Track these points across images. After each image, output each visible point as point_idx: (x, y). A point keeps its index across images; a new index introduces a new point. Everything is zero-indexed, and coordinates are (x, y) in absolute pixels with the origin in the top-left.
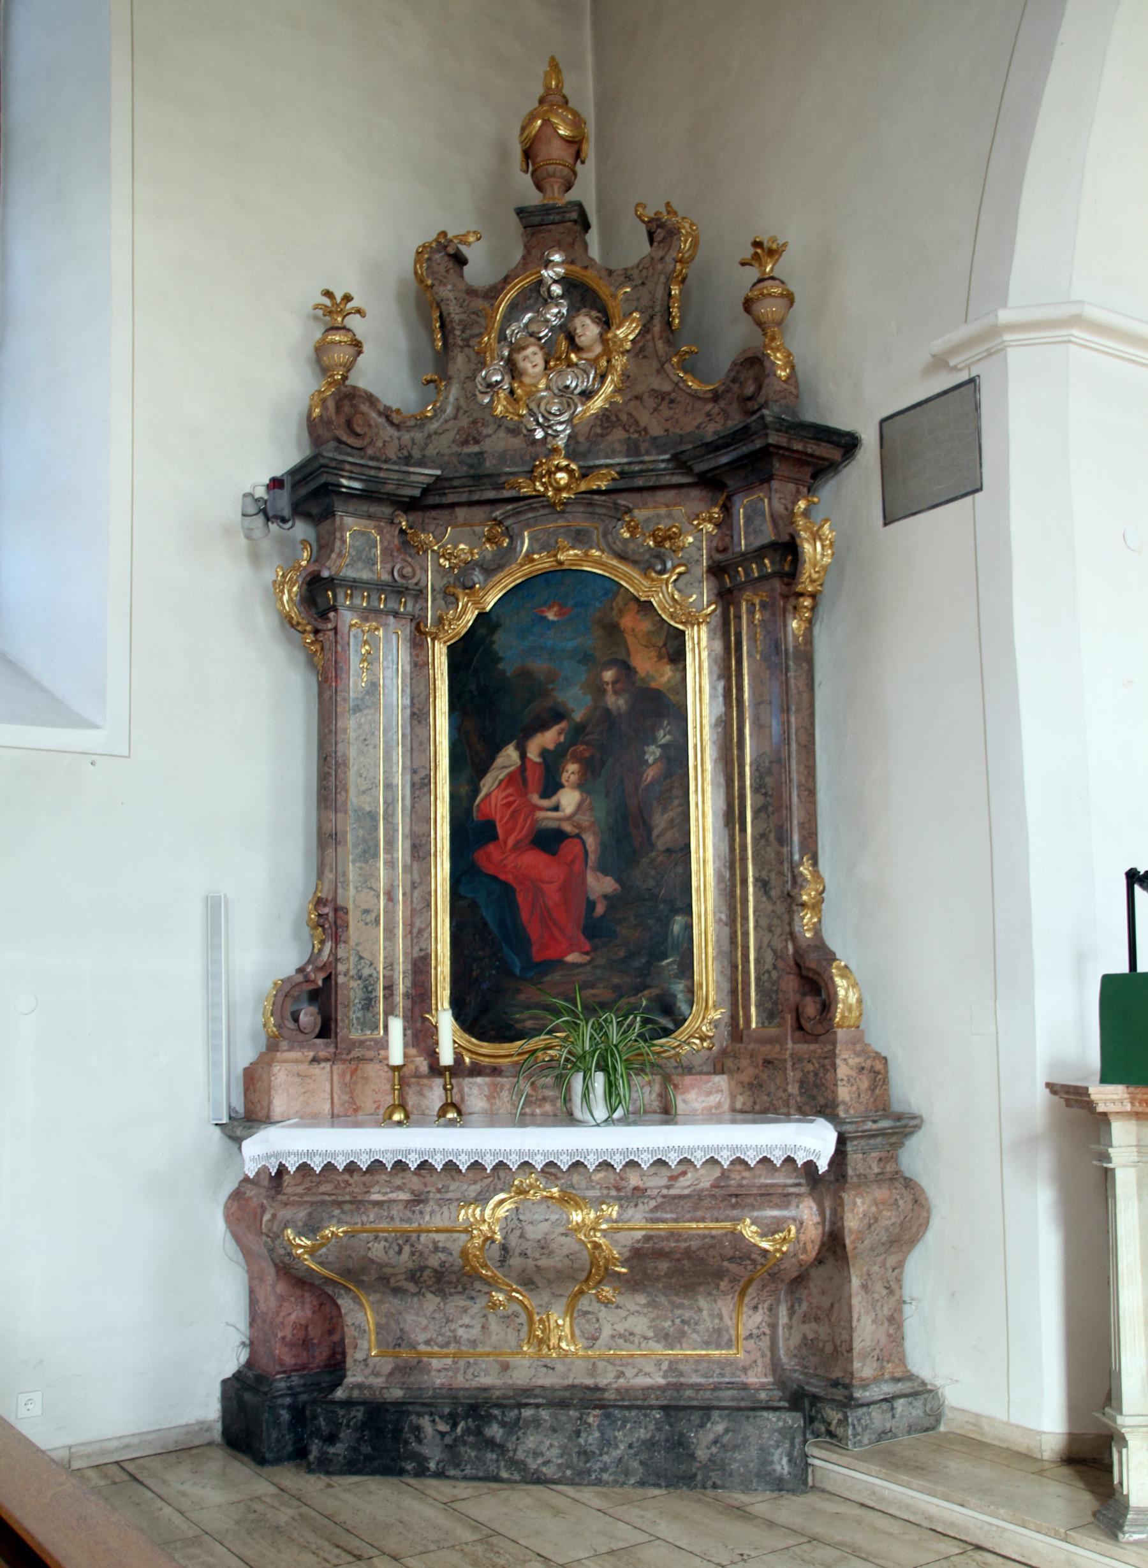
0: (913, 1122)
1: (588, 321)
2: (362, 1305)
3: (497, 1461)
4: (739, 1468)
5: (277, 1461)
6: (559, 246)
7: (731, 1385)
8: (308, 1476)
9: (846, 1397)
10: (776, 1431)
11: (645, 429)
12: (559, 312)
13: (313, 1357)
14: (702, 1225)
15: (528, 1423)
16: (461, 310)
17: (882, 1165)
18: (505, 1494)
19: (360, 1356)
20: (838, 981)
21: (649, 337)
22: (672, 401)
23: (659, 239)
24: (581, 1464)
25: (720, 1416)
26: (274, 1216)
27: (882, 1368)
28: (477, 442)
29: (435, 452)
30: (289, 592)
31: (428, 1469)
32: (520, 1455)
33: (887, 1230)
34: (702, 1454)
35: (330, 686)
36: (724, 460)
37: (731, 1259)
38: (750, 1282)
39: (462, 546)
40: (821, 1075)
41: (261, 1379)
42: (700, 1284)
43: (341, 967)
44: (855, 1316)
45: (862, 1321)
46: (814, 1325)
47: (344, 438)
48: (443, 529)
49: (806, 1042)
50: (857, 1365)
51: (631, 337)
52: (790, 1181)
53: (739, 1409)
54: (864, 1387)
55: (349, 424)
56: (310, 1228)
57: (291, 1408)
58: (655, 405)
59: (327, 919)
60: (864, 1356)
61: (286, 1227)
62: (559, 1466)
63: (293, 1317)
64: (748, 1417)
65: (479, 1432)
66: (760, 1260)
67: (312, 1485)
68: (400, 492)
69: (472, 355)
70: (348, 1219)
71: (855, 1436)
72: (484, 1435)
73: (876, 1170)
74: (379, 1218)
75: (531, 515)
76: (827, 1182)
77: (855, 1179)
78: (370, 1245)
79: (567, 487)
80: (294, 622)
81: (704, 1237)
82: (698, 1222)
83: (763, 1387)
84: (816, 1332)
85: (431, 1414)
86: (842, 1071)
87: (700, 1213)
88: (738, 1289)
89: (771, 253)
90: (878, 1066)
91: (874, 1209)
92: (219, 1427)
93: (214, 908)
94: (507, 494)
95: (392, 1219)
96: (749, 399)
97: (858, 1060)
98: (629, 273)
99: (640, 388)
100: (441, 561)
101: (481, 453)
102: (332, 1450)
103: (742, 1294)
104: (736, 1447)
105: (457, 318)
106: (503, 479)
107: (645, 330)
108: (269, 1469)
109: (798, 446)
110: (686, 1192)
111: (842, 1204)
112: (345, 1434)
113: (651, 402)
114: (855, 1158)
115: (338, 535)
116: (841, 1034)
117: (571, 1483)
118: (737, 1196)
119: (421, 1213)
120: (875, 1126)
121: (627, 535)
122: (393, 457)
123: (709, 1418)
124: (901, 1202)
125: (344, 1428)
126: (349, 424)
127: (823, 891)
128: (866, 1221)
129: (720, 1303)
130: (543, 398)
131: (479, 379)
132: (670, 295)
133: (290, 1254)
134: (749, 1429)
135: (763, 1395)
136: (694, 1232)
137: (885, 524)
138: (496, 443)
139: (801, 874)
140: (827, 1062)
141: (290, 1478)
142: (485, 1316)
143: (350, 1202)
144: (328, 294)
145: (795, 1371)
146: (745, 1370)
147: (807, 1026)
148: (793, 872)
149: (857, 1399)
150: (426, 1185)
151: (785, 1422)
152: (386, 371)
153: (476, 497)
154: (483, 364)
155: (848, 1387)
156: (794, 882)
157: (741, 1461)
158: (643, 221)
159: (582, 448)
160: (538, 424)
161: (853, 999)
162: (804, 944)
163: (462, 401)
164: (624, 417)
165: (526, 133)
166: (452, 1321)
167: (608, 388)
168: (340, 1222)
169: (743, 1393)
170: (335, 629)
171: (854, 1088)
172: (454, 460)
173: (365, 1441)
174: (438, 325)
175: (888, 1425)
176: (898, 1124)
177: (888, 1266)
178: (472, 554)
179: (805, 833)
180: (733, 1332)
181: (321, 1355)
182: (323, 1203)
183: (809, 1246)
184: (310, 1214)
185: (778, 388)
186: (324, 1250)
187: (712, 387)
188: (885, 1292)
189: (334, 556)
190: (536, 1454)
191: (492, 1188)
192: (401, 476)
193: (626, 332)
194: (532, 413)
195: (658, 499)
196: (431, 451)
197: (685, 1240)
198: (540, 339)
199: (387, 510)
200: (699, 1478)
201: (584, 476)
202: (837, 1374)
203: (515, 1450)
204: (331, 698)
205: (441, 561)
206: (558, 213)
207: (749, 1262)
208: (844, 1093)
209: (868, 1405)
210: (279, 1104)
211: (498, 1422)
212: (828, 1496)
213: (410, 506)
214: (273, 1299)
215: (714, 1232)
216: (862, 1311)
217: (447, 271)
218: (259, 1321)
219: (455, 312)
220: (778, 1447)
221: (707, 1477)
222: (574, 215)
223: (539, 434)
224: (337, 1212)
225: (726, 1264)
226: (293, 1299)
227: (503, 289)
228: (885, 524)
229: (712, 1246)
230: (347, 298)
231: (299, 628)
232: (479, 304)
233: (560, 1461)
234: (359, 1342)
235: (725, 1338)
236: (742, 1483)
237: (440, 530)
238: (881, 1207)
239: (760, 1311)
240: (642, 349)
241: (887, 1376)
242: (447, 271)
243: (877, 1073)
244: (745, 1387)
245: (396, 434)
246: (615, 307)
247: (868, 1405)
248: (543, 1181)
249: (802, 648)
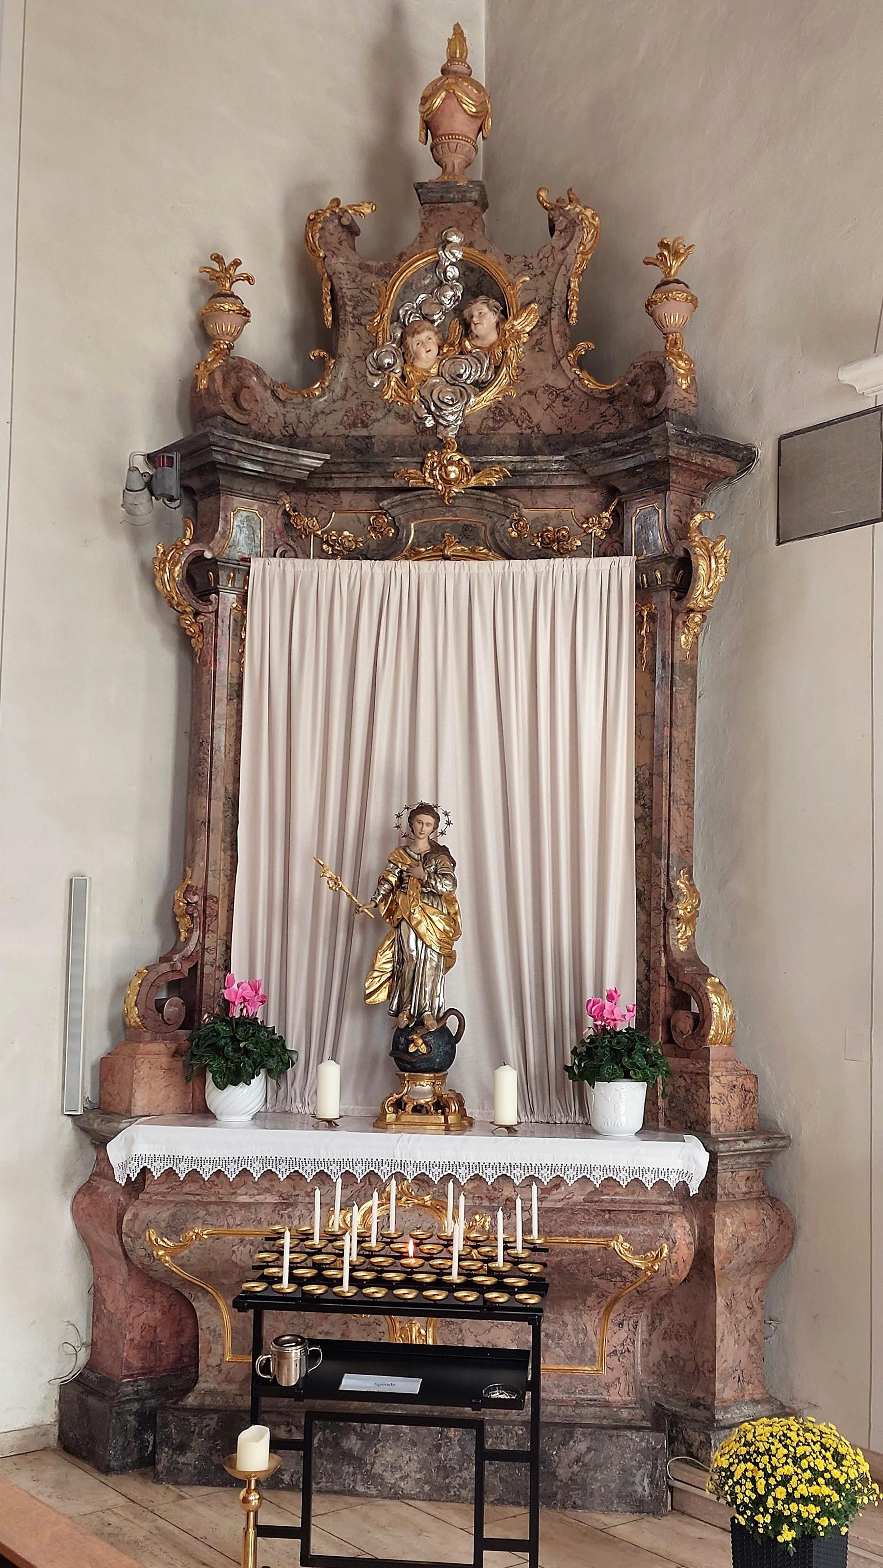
0: (782, 1143)
1: (485, 309)
2: (218, 1308)
3: (354, 1474)
4: (600, 1488)
5: (123, 1470)
6: (459, 228)
7: (592, 1403)
8: (155, 1486)
9: (708, 1419)
10: (638, 1451)
11: (538, 426)
12: (454, 296)
13: (161, 1360)
14: (574, 1240)
15: (387, 1435)
16: (354, 285)
17: (749, 1184)
18: (364, 1509)
19: (213, 1361)
20: (713, 998)
21: (545, 329)
22: (566, 399)
23: (561, 228)
24: (440, 1480)
25: (583, 1434)
26: (136, 1216)
27: (743, 1389)
28: (365, 426)
29: (321, 433)
30: (171, 572)
31: (282, 1481)
32: (378, 1469)
33: (754, 1251)
34: (563, 1473)
35: (210, 669)
36: (621, 466)
37: (601, 1276)
38: (616, 1300)
39: (346, 533)
40: (693, 1091)
41: (106, 1382)
42: (566, 1299)
43: (208, 957)
44: (719, 1336)
45: (725, 1342)
46: (675, 1343)
47: (231, 414)
48: (327, 513)
49: (676, 1056)
50: (718, 1386)
51: (528, 329)
52: (663, 1200)
53: (602, 1427)
54: (726, 1409)
55: (236, 398)
56: (174, 1229)
57: (139, 1415)
58: (548, 402)
59: (195, 908)
61: (148, 1227)
62: (417, 1481)
63: (143, 1317)
64: (611, 1436)
65: (337, 1444)
66: (630, 1277)
67: (160, 1496)
68: (286, 474)
69: (363, 333)
70: (214, 1221)
72: (342, 1448)
73: (744, 1189)
74: (246, 1221)
75: (418, 506)
76: (703, 1201)
77: (724, 1198)
78: (235, 1248)
79: (457, 481)
80: (174, 603)
81: (577, 1252)
82: (570, 1237)
83: (625, 1406)
84: (677, 1350)
85: (288, 1425)
86: (715, 1088)
87: (574, 1228)
88: (604, 1304)
89: (676, 255)
90: (749, 1085)
91: (742, 1229)
92: (55, 1430)
93: (77, 891)
94: (395, 483)
95: (260, 1222)
96: (648, 405)
97: (730, 1078)
98: (529, 260)
99: (534, 383)
100: (325, 546)
101: (370, 437)
102: (182, 1460)
103: (609, 1309)
104: (598, 1467)
105: (349, 293)
106: (393, 469)
107: (544, 321)
108: (112, 1479)
109: (697, 459)
110: (559, 1205)
111: (712, 1224)
112: (197, 1443)
113: (545, 399)
114: (723, 1175)
115: (222, 515)
116: (715, 1052)
117: (429, 1499)
118: (610, 1211)
119: (289, 1217)
120: (746, 1146)
121: (514, 534)
122: (277, 434)
123: (572, 1437)
124: (767, 1223)
125: (196, 1436)
126: (236, 398)
127: (698, 906)
128: (734, 1242)
129: (585, 1317)
130: (434, 385)
131: (369, 359)
132: (569, 287)
133: (150, 1255)
134: (610, 1448)
135: (625, 1414)
136: (567, 1246)
137: (778, 543)
138: (386, 428)
139: (678, 888)
140: (699, 1078)
141: (134, 1486)
142: (346, 1323)
143: (215, 1203)
144: (218, 259)
145: (654, 1388)
146: (607, 1387)
147: (679, 1041)
148: (668, 884)
149: (718, 1421)
150: (294, 1189)
151: (648, 1442)
152: (264, 334)
153: (363, 484)
154: (375, 345)
155: (710, 1408)
156: (670, 897)
157: (604, 1480)
158: (545, 208)
159: (474, 441)
160: (430, 412)
161: (726, 1014)
162: (677, 957)
163: (351, 382)
164: (517, 412)
165: (427, 106)
166: (312, 1327)
167: (503, 378)
168: (204, 1223)
169: (605, 1411)
170: (217, 611)
171: (726, 1106)
172: (341, 442)
173: (218, 1451)
174: (329, 298)
176: (768, 1144)
177: (752, 1286)
178: (356, 542)
179: (683, 847)
180: (596, 1348)
181: (169, 1357)
182: (187, 1203)
183: (681, 1266)
184: (174, 1215)
185: (678, 397)
186: (186, 1252)
187: (608, 387)
188: (747, 1312)
189: (217, 535)
190: (394, 1468)
191: (363, 1193)
192: (289, 458)
193: (524, 323)
194: (423, 400)
195: (548, 499)
196: (317, 431)
197: (557, 1255)
198: (433, 322)
199: (273, 492)
200: (559, 1497)
201: (476, 471)
202: (698, 1393)
203: (373, 1464)
204: (209, 682)
205: (325, 546)
206: (458, 192)
207: (619, 1279)
208: (715, 1111)
210: (140, 1101)
211: (356, 1434)
212: (689, 1519)
213: (298, 487)
214: (122, 1299)
215: (586, 1248)
217: (340, 243)
218: (105, 1321)
219: (347, 287)
220: (640, 1468)
221: (568, 1497)
222: (475, 195)
223: (429, 423)
224: (202, 1213)
225: (596, 1279)
226: (143, 1299)
227: (398, 266)
228: (778, 543)
229: (584, 1262)
230: (237, 263)
231: (179, 609)
232: (372, 280)
233: (418, 1476)
234: (213, 1346)
235: (589, 1353)
236: (602, 1504)
237: (324, 514)
238: (749, 1228)
239: (626, 1328)
240: (538, 342)
241: (747, 1398)
242: (340, 243)
243: (750, 1093)
244: (607, 1404)
245: (283, 410)
246: (515, 296)
248: (415, 1188)
249: (688, 662)
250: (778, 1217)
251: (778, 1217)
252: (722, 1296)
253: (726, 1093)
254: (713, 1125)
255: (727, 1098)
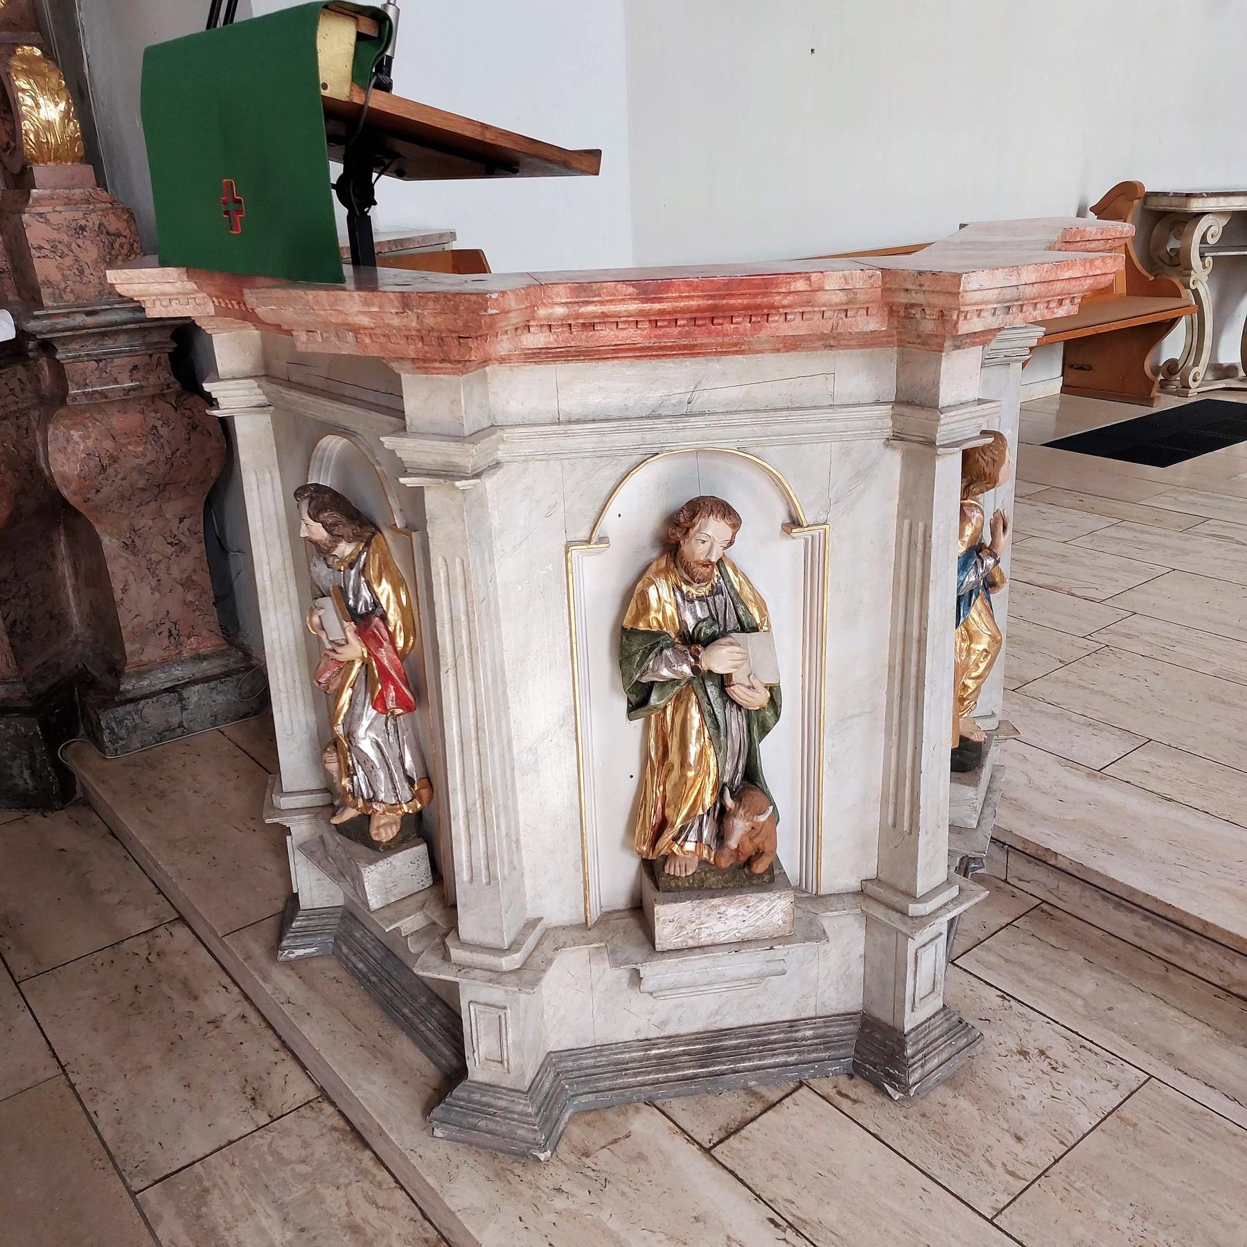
44: (117, 586)
54: (140, 675)
60: (142, 634)
71: (114, 742)
91: (108, 444)
151: (16, 729)
171: (69, 261)
175: (175, 721)
209: (135, 700)
216: (131, 579)
220: (14, 758)
247: (135, 700)
250: (186, 421)
251: (186, 421)
252: (111, 535)
253: (66, 239)
254: (45, 292)
255: (69, 246)
